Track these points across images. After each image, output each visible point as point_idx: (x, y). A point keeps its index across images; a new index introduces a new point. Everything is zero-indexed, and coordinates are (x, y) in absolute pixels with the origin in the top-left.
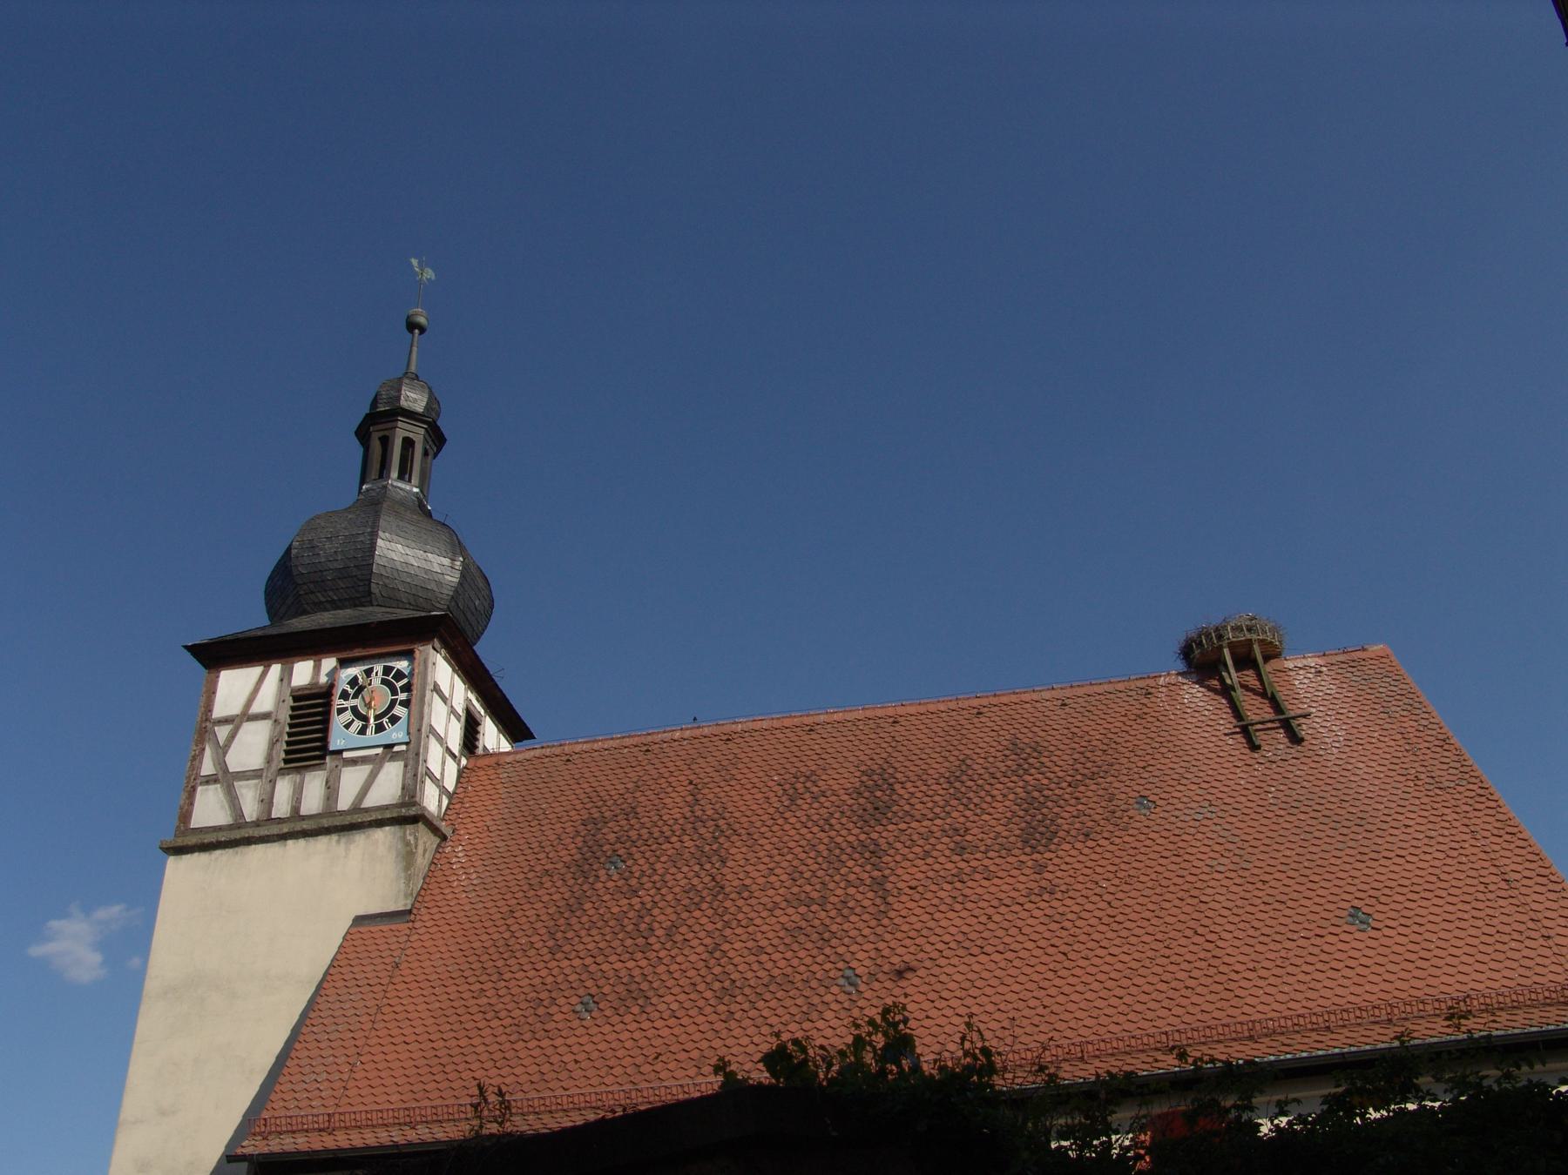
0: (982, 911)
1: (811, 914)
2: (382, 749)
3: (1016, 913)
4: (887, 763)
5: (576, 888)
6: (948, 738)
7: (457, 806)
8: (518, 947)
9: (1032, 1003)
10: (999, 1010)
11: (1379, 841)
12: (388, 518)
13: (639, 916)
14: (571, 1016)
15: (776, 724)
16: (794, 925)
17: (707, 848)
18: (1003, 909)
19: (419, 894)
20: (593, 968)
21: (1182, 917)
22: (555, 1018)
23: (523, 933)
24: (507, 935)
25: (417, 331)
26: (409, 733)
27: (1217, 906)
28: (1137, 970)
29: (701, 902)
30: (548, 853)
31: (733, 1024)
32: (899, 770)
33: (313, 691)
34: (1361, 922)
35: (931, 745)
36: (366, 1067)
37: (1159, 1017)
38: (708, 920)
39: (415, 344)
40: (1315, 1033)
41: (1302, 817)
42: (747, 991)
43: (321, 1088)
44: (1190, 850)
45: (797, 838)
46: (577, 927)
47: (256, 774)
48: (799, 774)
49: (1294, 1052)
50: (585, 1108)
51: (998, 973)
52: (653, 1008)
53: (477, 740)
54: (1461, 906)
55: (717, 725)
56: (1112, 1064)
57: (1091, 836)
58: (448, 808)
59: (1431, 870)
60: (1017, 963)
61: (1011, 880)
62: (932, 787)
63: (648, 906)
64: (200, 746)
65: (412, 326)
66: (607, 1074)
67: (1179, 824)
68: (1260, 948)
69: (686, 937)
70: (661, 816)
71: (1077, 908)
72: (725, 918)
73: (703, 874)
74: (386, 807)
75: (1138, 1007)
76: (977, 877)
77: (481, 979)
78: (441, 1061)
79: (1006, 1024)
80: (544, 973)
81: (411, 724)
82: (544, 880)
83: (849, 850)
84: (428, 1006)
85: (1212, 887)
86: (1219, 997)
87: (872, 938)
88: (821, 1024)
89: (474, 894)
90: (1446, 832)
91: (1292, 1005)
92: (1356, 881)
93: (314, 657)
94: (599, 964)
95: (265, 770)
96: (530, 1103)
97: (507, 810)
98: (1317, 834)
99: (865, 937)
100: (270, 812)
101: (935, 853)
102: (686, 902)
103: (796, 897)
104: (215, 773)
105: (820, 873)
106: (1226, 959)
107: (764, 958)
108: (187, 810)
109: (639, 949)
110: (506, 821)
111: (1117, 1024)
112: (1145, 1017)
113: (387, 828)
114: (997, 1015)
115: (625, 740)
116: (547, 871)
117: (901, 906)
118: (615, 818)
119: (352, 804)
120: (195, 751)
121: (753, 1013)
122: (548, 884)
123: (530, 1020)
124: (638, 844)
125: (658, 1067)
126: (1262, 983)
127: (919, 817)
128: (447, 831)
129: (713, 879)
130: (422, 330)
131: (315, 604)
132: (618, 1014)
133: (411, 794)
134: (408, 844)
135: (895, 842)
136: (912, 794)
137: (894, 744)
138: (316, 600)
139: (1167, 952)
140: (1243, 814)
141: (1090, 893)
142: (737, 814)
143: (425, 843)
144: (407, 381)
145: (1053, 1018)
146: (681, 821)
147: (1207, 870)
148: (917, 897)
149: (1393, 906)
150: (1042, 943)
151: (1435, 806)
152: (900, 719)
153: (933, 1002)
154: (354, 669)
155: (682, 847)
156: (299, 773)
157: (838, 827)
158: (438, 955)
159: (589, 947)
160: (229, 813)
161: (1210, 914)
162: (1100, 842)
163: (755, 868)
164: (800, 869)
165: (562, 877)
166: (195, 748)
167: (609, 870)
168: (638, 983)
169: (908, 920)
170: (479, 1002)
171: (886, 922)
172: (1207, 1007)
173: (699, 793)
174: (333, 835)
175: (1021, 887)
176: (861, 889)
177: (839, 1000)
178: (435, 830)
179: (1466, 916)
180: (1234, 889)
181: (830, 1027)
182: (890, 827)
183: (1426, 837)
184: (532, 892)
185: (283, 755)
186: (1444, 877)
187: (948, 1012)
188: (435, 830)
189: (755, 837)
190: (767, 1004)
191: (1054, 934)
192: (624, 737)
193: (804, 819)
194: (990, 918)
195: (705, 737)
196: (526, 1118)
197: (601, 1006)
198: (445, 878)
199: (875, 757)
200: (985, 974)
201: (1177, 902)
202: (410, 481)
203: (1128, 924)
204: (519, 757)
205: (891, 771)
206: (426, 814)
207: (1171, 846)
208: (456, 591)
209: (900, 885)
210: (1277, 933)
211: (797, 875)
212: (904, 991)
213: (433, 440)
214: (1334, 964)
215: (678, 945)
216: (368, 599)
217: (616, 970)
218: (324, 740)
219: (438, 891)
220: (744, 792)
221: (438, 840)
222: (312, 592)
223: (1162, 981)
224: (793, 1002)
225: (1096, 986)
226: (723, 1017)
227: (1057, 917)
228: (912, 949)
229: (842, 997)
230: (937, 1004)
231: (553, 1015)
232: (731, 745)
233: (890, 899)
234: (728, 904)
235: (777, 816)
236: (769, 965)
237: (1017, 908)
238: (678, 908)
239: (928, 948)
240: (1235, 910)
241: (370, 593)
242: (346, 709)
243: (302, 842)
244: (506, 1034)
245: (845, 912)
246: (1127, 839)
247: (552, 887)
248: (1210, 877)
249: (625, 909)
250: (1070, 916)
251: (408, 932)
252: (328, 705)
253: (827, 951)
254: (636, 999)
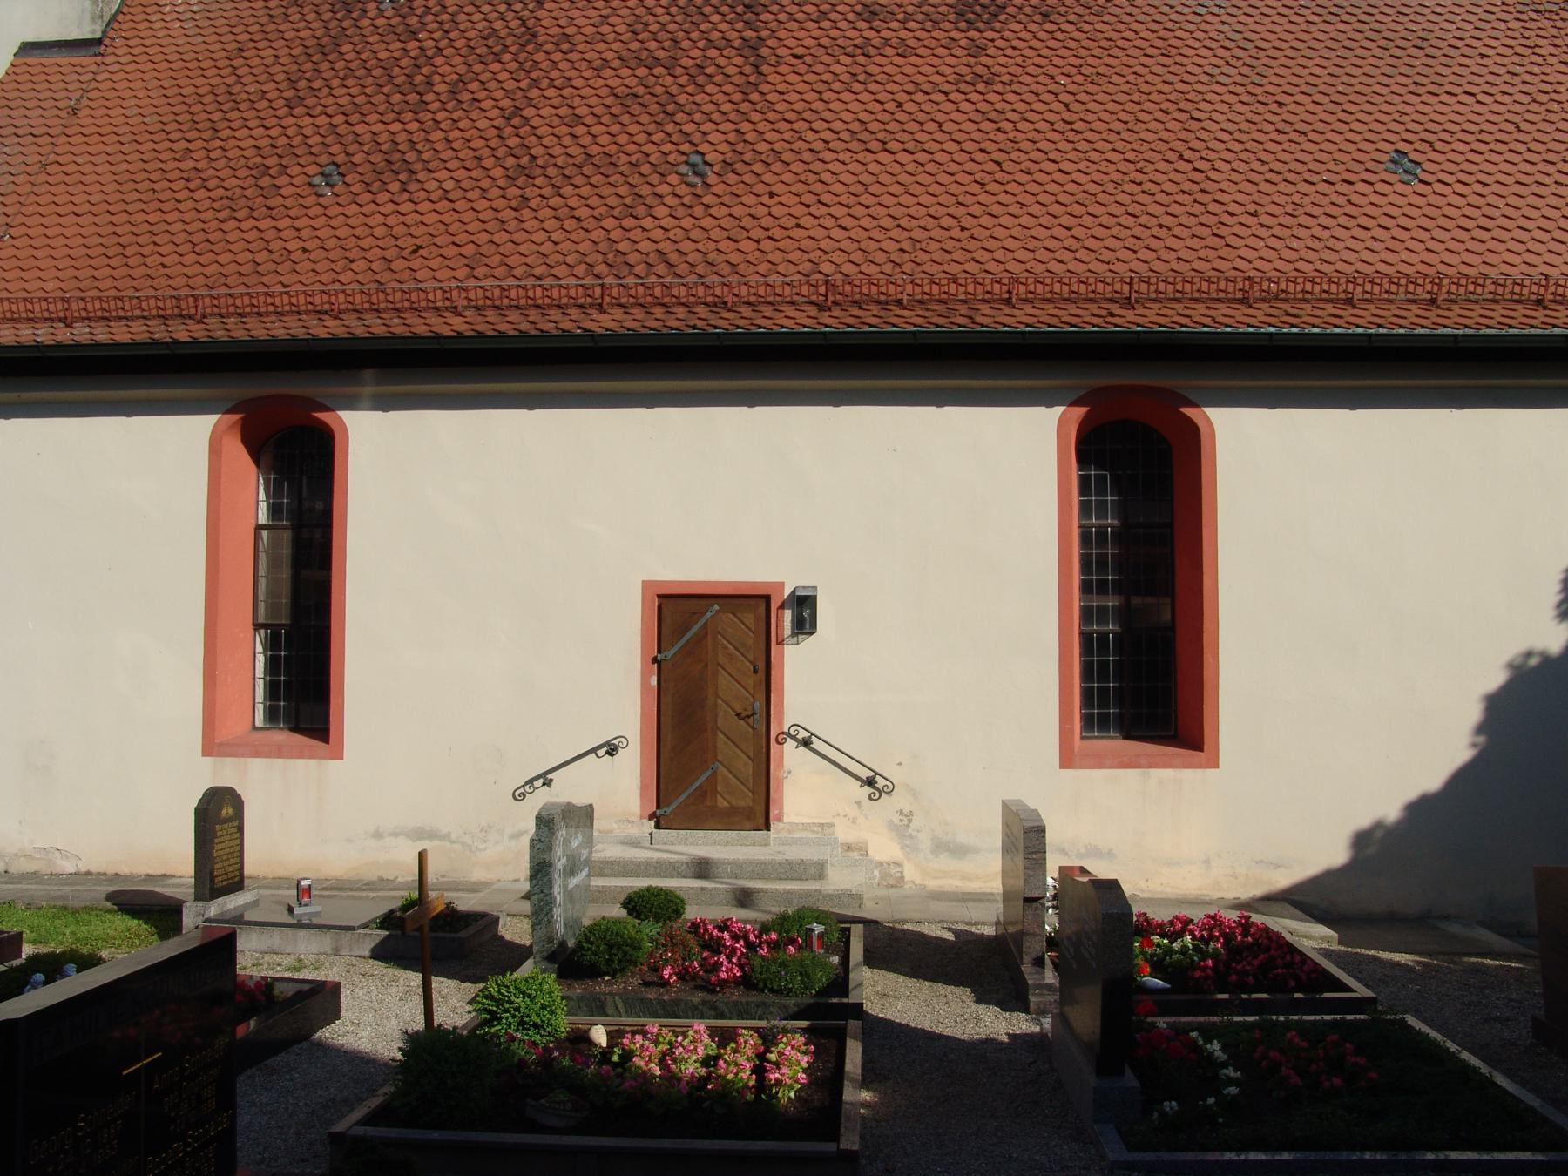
0: (890, 96)
3: (938, 104)
8: (245, 96)
9: (946, 222)
10: (899, 226)
11: (1444, 71)
13: (415, 65)
14: (307, 190)
16: (628, 91)
18: (919, 97)
20: (343, 129)
21: (1165, 135)
22: (283, 192)
23: (254, 79)
24: (231, 80)
27: (1214, 127)
28: (1094, 195)
31: (526, 214)
34: (1405, 171)
36: (17, 243)
37: (1118, 260)
40: (1331, 305)
41: (1342, 27)
42: (551, 171)
44: (1184, 51)
49: (1302, 325)
50: (307, 312)
51: (904, 178)
52: (419, 186)
54: (1541, 166)
56: (1049, 312)
57: (1051, 18)
59: (1509, 116)
60: (931, 168)
61: (935, 61)
63: (430, 53)
67: (1174, 17)
68: (1265, 187)
69: (476, 96)
71: (1021, 107)
72: (534, 75)
73: (510, 16)
75: (1090, 243)
76: (889, 51)
77: (188, 136)
78: (121, 240)
79: (906, 245)
84: (112, 168)
85: (1209, 102)
86: (1203, 243)
87: (733, 116)
89: (191, 24)
90: (1536, 70)
91: (1301, 265)
92: (1405, 119)
98: (1359, 52)
101: (833, 16)
102: (482, 51)
105: (672, 27)
106: (1219, 196)
107: (580, 130)
111: (1061, 262)
112: (1100, 257)
114: (895, 233)
125: (416, 264)
126: (1263, 232)
129: (524, 24)
132: (369, 191)
139: (1139, 177)
140: (1262, 14)
141: (1041, 89)
145: (973, 245)
147: (1205, 79)
148: (802, 69)
149: (1452, 156)
150: (969, 146)
151: (1527, 33)
153: (808, 206)
158: (134, 101)
159: (341, 101)
161: (1204, 135)
162: (1063, 27)
164: (644, 20)
168: (403, 153)
169: (786, 97)
170: (182, 165)
171: (755, 97)
172: (1184, 254)
175: (947, 70)
176: (725, 52)
177: (678, 193)
179: (1547, 180)
180: (1239, 108)
181: (660, 227)
183: (1508, 72)
184: (273, 27)
186: (1524, 126)
187: (828, 222)
191: (986, 137)
194: (900, 105)
196: (224, 320)
197: (349, 179)
200: (885, 178)
201: (1159, 115)
203: (1089, 135)
207: (1160, 43)
209: (781, 52)
210: (1290, 171)
211: (639, 27)
214: (1363, 221)
215: (464, 106)
217: (374, 134)
219: (142, 17)
223: (1128, 214)
224: (612, 190)
225: (1035, 209)
226: (514, 204)
227: (993, 115)
228: (787, 136)
230: (813, 210)
231: (280, 188)
236: (586, 140)
237: (939, 97)
238: (470, 58)
239: (810, 136)
240: (1237, 135)
244: (214, 209)
245: (701, 79)
246: (1099, 26)
247: (300, 21)
248: (1208, 88)
249: (396, 55)
250: (1011, 116)
251: (94, 68)
253: (670, 128)
254: (397, 173)
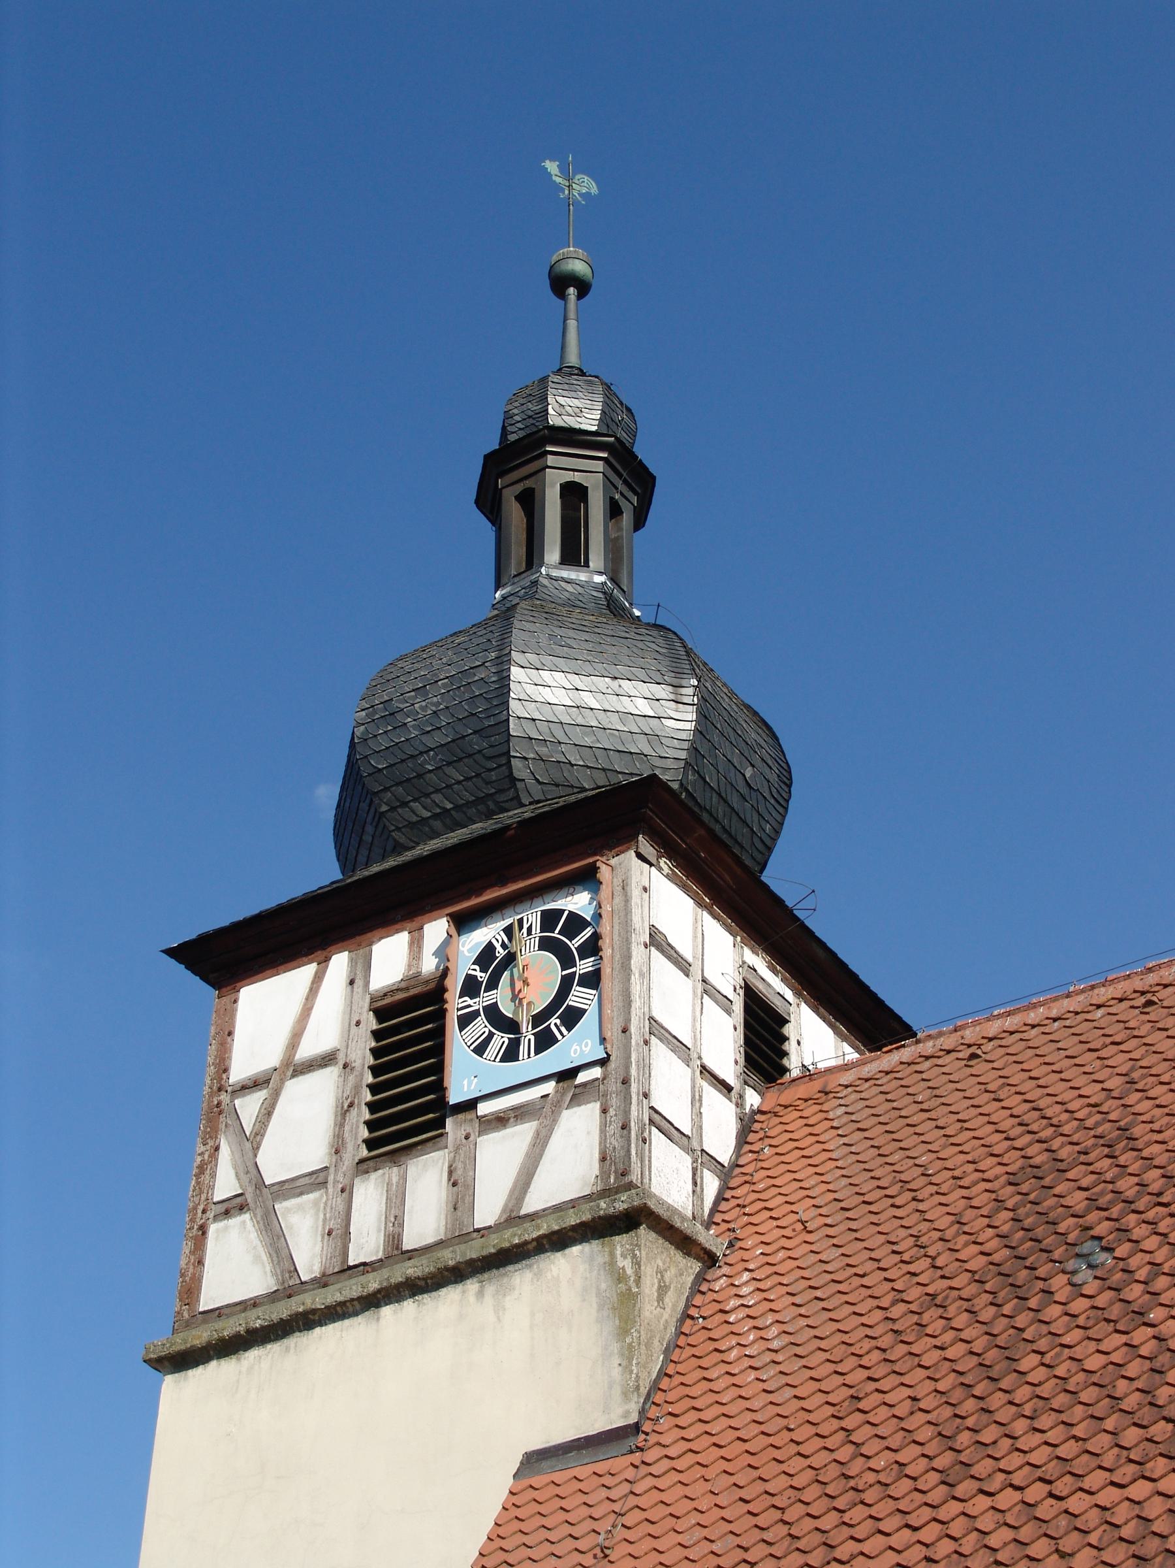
5: (1000, 1325)
12: (528, 626)
19: (655, 1387)
20: (1047, 1509)
25: (572, 291)
26: (603, 1040)
30: (934, 1258)
33: (412, 992)
47: (316, 1180)
53: (785, 1054)
58: (720, 1198)
64: (211, 1143)
65: (560, 283)
74: (573, 1204)
81: (605, 1018)
82: (926, 1318)
94: (1060, 1498)
95: (332, 1170)
104: (240, 1191)
108: (194, 1275)
110: (843, 1205)
113: (575, 1250)
115: (1096, 991)
116: (933, 1296)
118: (1083, 1158)
119: (504, 1211)
120: (202, 1154)
122: (937, 1326)
124: (1140, 1205)
130: (583, 288)
131: (411, 825)
133: (621, 1167)
134: (620, 1277)
138: (415, 819)
143: (661, 1272)
144: (557, 379)
156: (396, 1163)
159: (1035, 1458)
160: (268, 1268)
165: (966, 1305)
166: (203, 1148)
174: (469, 1282)
178: (684, 1242)
184: (902, 1349)
185: (365, 1133)
188: (684, 1242)
192: (1093, 987)
198: (712, 1345)
202: (587, 565)
206: (652, 1205)
208: (694, 750)
213: (625, 482)
216: (511, 793)
217: (1104, 1509)
218: (439, 1087)
221: (696, 1266)
222: (405, 804)
241: (513, 780)
242: (476, 1014)
243: (409, 1306)
249: (1116, 1357)
251: (630, 1473)
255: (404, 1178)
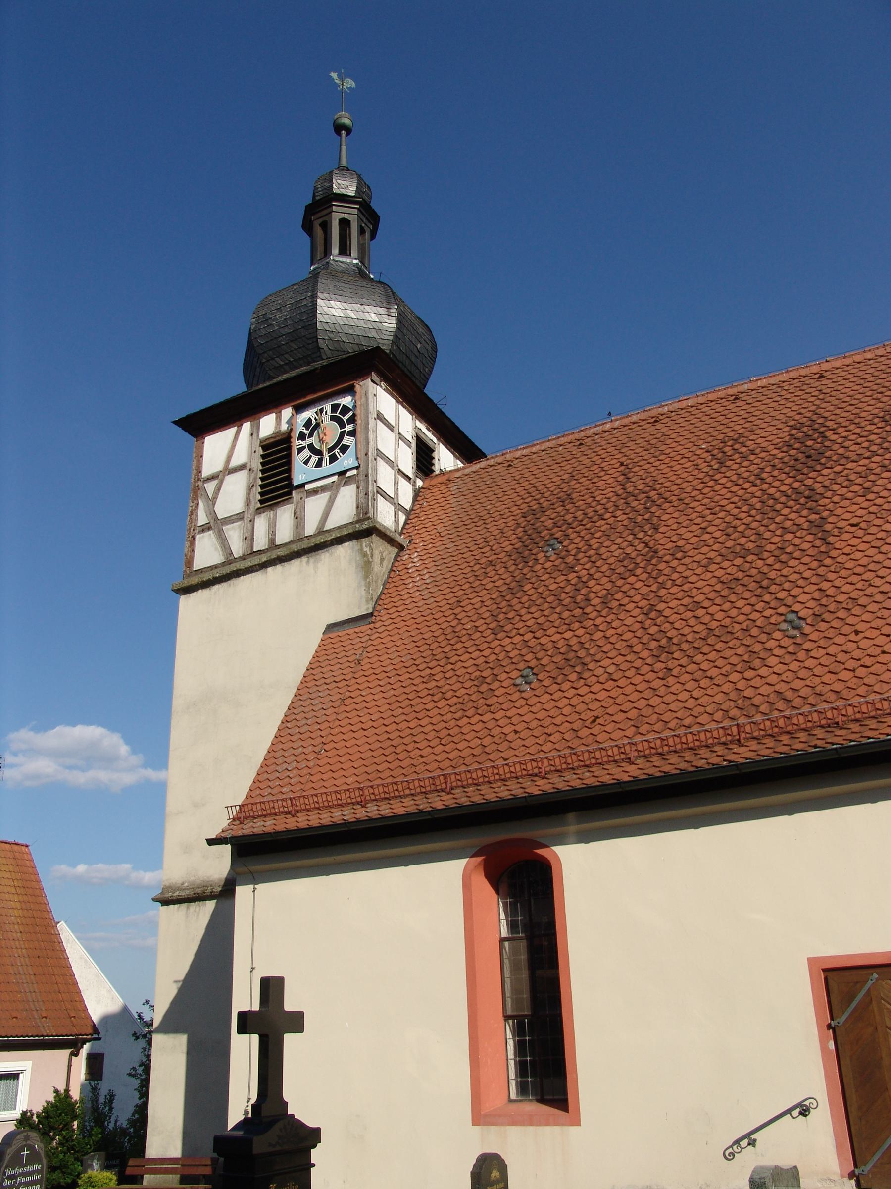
1: (748, 565)
2: (337, 476)
4: (817, 414)
6: (879, 381)
7: (413, 521)
13: (576, 589)
14: (512, 690)
15: (701, 400)
16: (730, 577)
17: (639, 518)
19: (379, 598)
22: (496, 693)
26: (357, 458)
29: (636, 568)
30: (491, 547)
32: (829, 418)
33: (277, 439)
35: (861, 391)
38: (643, 584)
39: (343, 143)
42: (685, 646)
43: (291, 776)
45: (728, 496)
46: (517, 607)
47: (239, 517)
48: (726, 439)
55: (645, 411)
58: (406, 523)
62: (867, 428)
63: (584, 579)
64: (195, 502)
65: (339, 128)
66: (546, 742)
69: (621, 602)
70: (595, 498)
72: (660, 580)
73: (636, 542)
74: (346, 526)
80: (487, 652)
83: (783, 499)
88: (764, 671)
93: (275, 410)
96: (458, 777)
97: (456, 516)
99: (807, 579)
100: (252, 547)
102: (621, 570)
103: (731, 550)
109: (577, 619)
113: (346, 544)
116: (491, 562)
117: (844, 544)
118: (552, 507)
119: (317, 529)
121: (691, 668)
123: (473, 697)
124: (574, 525)
127: (855, 458)
128: (405, 543)
129: (647, 545)
130: (349, 131)
131: (275, 368)
132: (556, 683)
133: (365, 510)
134: (365, 555)
135: (831, 484)
136: (845, 437)
137: (821, 397)
138: (277, 365)
142: (667, 484)
143: (381, 553)
144: (337, 172)
146: (613, 499)
148: (860, 533)
152: (825, 374)
154: (307, 412)
155: (615, 521)
156: (272, 509)
157: (770, 479)
163: (688, 529)
164: (733, 524)
167: (547, 552)
168: (576, 652)
169: (852, 556)
171: (828, 561)
173: (629, 472)
176: (798, 534)
177: (783, 645)
178: (391, 541)
181: (774, 673)
182: (825, 472)
188: (391, 541)
189: (686, 501)
190: (706, 657)
192: (559, 438)
193: (734, 478)
195: (634, 423)
196: (466, 790)
197: (540, 677)
198: (402, 582)
199: (803, 411)
204: (467, 471)
205: (821, 421)
206: (378, 526)
209: (840, 524)
211: (730, 530)
212: (853, 628)
213: (367, 219)
216: (318, 354)
218: (289, 478)
220: (673, 463)
221: (396, 551)
222: (273, 359)
224: (733, 652)
228: (859, 586)
229: (785, 642)
232: (659, 426)
233: (831, 539)
234: (662, 566)
235: (707, 479)
236: (706, 619)
238: (613, 577)
242: (304, 447)
245: (784, 557)
249: (562, 585)
251: (369, 632)
252: (289, 448)
253: (767, 597)
255: (275, 516)
